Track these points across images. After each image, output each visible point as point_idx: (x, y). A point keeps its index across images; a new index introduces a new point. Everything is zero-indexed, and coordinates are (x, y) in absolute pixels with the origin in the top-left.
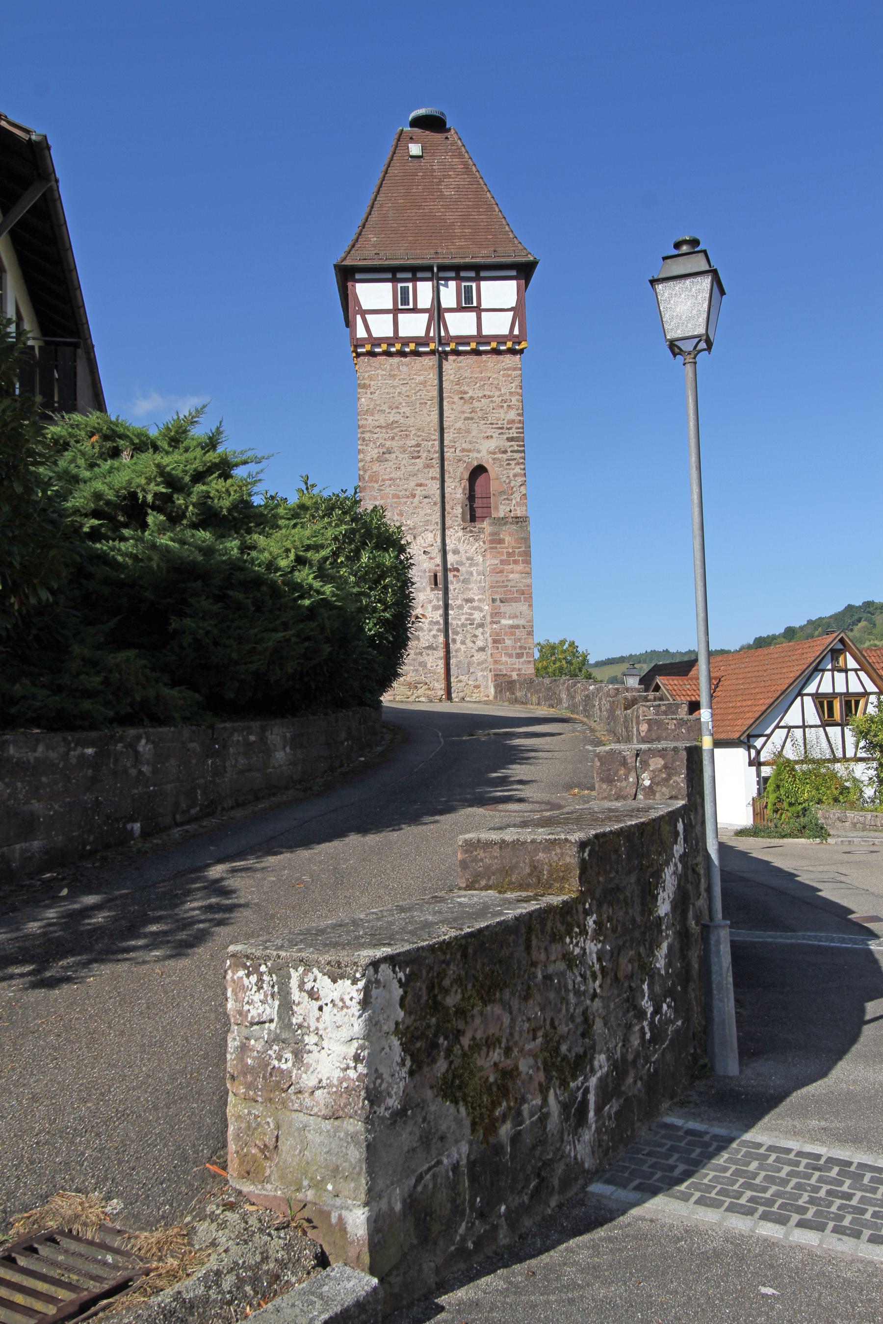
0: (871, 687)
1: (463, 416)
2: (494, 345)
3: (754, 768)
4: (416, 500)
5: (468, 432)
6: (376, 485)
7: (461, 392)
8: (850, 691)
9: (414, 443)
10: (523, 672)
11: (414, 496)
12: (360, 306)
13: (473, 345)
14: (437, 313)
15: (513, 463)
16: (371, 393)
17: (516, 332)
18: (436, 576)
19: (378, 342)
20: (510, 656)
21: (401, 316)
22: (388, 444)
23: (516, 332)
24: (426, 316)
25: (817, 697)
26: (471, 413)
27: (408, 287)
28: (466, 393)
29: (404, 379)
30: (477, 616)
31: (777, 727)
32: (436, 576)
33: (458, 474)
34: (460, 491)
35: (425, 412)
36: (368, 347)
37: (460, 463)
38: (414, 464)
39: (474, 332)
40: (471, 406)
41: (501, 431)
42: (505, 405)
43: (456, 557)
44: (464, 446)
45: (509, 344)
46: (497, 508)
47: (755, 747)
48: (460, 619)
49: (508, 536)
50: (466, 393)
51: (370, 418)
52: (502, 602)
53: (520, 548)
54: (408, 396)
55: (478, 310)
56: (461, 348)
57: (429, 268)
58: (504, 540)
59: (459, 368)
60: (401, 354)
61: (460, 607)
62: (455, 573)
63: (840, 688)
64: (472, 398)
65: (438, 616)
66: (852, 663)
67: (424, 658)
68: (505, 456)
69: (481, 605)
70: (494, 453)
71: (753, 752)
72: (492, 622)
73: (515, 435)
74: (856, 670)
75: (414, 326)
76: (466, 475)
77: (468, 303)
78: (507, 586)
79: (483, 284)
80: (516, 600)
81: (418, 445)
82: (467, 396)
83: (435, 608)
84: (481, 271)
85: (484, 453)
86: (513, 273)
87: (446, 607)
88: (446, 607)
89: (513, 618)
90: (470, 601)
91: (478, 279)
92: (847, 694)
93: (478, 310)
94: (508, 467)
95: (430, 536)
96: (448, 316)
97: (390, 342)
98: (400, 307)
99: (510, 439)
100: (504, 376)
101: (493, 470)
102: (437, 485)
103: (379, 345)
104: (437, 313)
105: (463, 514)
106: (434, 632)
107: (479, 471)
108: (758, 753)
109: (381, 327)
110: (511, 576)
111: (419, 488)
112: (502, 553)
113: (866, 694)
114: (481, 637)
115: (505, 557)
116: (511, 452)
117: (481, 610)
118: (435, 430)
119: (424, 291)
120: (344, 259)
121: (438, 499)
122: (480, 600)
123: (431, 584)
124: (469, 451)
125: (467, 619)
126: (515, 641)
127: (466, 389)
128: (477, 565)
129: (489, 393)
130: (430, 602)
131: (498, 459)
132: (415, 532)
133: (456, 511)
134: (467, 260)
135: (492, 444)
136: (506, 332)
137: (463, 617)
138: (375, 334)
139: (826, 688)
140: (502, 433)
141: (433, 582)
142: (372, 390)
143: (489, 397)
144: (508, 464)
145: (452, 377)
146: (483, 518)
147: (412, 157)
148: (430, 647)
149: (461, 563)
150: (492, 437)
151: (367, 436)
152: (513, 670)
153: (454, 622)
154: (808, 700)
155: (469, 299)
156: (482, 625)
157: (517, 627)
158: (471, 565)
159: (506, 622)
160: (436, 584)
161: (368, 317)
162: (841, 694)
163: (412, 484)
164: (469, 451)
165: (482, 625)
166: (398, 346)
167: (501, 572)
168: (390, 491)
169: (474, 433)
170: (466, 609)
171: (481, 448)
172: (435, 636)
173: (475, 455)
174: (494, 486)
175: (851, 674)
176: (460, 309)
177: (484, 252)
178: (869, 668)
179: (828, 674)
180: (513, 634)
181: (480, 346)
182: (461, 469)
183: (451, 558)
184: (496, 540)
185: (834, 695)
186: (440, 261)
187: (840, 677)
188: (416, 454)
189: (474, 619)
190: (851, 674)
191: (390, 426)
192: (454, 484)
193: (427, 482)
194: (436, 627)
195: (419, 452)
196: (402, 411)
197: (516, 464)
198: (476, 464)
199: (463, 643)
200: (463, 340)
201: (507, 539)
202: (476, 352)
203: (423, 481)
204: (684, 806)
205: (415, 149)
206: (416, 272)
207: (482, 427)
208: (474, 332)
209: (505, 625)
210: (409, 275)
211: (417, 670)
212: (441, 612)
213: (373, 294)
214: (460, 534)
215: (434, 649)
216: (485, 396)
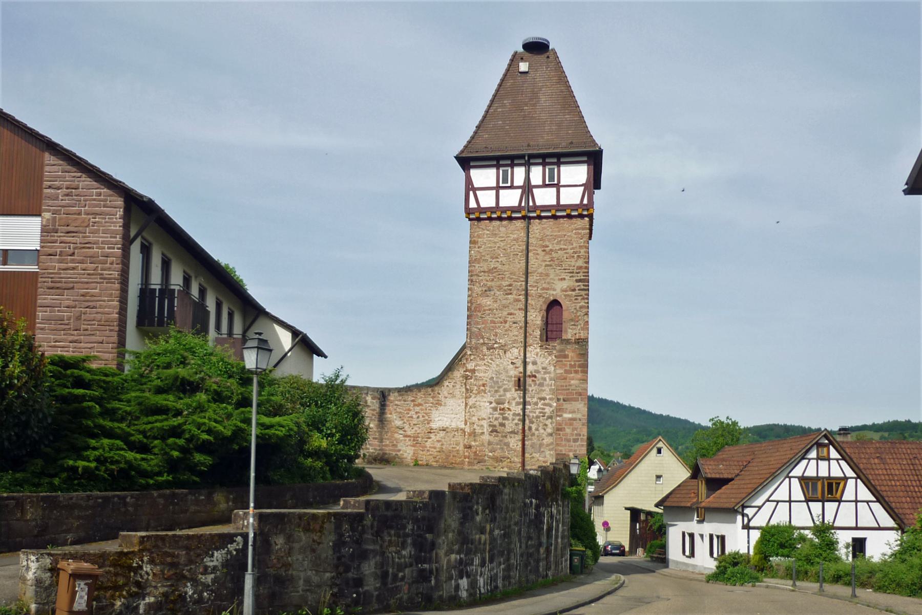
0: (850, 473)
1: (544, 264)
2: (568, 211)
3: (746, 531)
4: (507, 325)
5: (547, 275)
6: (479, 314)
7: (544, 246)
8: (832, 475)
9: (507, 283)
11: (506, 322)
12: (473, 185)
13: (553, 212)
14: (527, 189)
15: (580, 298)
17: (585, 202)
18: (519, 380)
19: (484, 210)
21: (501, 192)
22: (489, 284)
23: (585, 202)
24: (520, 191)
25: (803, 480)
30: (548, 410)
31: (768, 500)
32: (519, 380)
33: (538, 307)
34: (540, 318)
35: (517, 261)
36: (477, 215)
37: (541, 299)
38: (507, 299)
39: (554, 203)
43: (535, 367)
44: (544, 285)
46: (566, 332)
47: (747, 516)
49: (571, 353)
51: (477, 265)
52: (564, 400)
55: (558, 186)
56: (543, 214)
57: (522, 157)
59: (544, 228)
60: (500, 219)
61: (536, 404)
63: (823, 473)
64: (551, 250)
65: (519, 409)
66: (834, 454)
67: (508, 440)
68: (574, 293)
70: (566, 291)
71: (746, 519)
72: (557, 416)
74: (837, 460)
75: (510, 198)
76: (545, 307)
80: (576, 400)
81: (510, 285)
82: (547, 249)
83: (518, 404)
85: (558, 290)
86: (585, 159)
87: (525, 403)
88: (525, 403)
90: (544, 399)
91: (559, 164)
92: (829, 478)
93: (558, 186)
95: (515, 351)
96: (535, 190)
97: (491, 210)
98: (501, 185)
99: (577, 281)
100: (575, 234)
101: (565, 303)
102: (522, 314)
103: (505, 212)
104: (527, 189)
105: (541, 335)
106: (516, 421)
107: (554, 305)
108: (749, 520)
109: (487, 200)
110: (572, 382)
112: (565, 365)
113: (846, 479)
114: (550, 426)
115: (568, 368)
117: (551, 406)
119: (519, 174)
120: (462, 152)
121: (522, 324)
122: (550, 399)
124: (548, 289)
126: (574, 429)
127: (547, 243)
128: (549, 373)
129: (562, 247)
130: (514, 399)
131: (568, 295)
133: (536, 333)
135: (565, 285)
136: (578, 202)
137: (537, 411)
138: (482, 205)
139: (811, 472)
145: (537, 235)
146: (554, 339)
147: (521, 73)
148: (513, 432)
149: (538, 372)
150: (564, 279)
152: (570, 451)
153: (531, 415)
154: (795, 483)
155: (552, 178)
156: (550, 417)
157: (574, 419)
158: (545, 373)
159: (567, 416)
160: (519, 386)
161: (478, 192)
162: (823, 478)
163: (505, 313)
164: (548, 289)
165: (550, 417)
166: (499, 214)
167: (565, 379)
168: (489, 318)
170: (540, 405)
171: (556, 287)
172: (516, 424)
173: (552, 292)
174: (566, 315)
175: (833, 463)
176: (545, 185)
178: (847, 458)
179: (813, 462)
180: (571, 424)
182: (541, 303)
183: (530, 368)
184: (562, 356)
185: (818, 478)
187: (823, 465)
190: (833, 463)
191: (490, 271)
198: (552, 298)
199: (537, 429)
202: (555, 217)
203: (512, 311)
204: (123, 531)
205: (523, 67)
206: (513, 160)
207: (558, 272)
208: (554, 203)
210: (509, 162)
211: (502, 449)
212: (521, 407)
213: (484, 177)
214: (538, 350)
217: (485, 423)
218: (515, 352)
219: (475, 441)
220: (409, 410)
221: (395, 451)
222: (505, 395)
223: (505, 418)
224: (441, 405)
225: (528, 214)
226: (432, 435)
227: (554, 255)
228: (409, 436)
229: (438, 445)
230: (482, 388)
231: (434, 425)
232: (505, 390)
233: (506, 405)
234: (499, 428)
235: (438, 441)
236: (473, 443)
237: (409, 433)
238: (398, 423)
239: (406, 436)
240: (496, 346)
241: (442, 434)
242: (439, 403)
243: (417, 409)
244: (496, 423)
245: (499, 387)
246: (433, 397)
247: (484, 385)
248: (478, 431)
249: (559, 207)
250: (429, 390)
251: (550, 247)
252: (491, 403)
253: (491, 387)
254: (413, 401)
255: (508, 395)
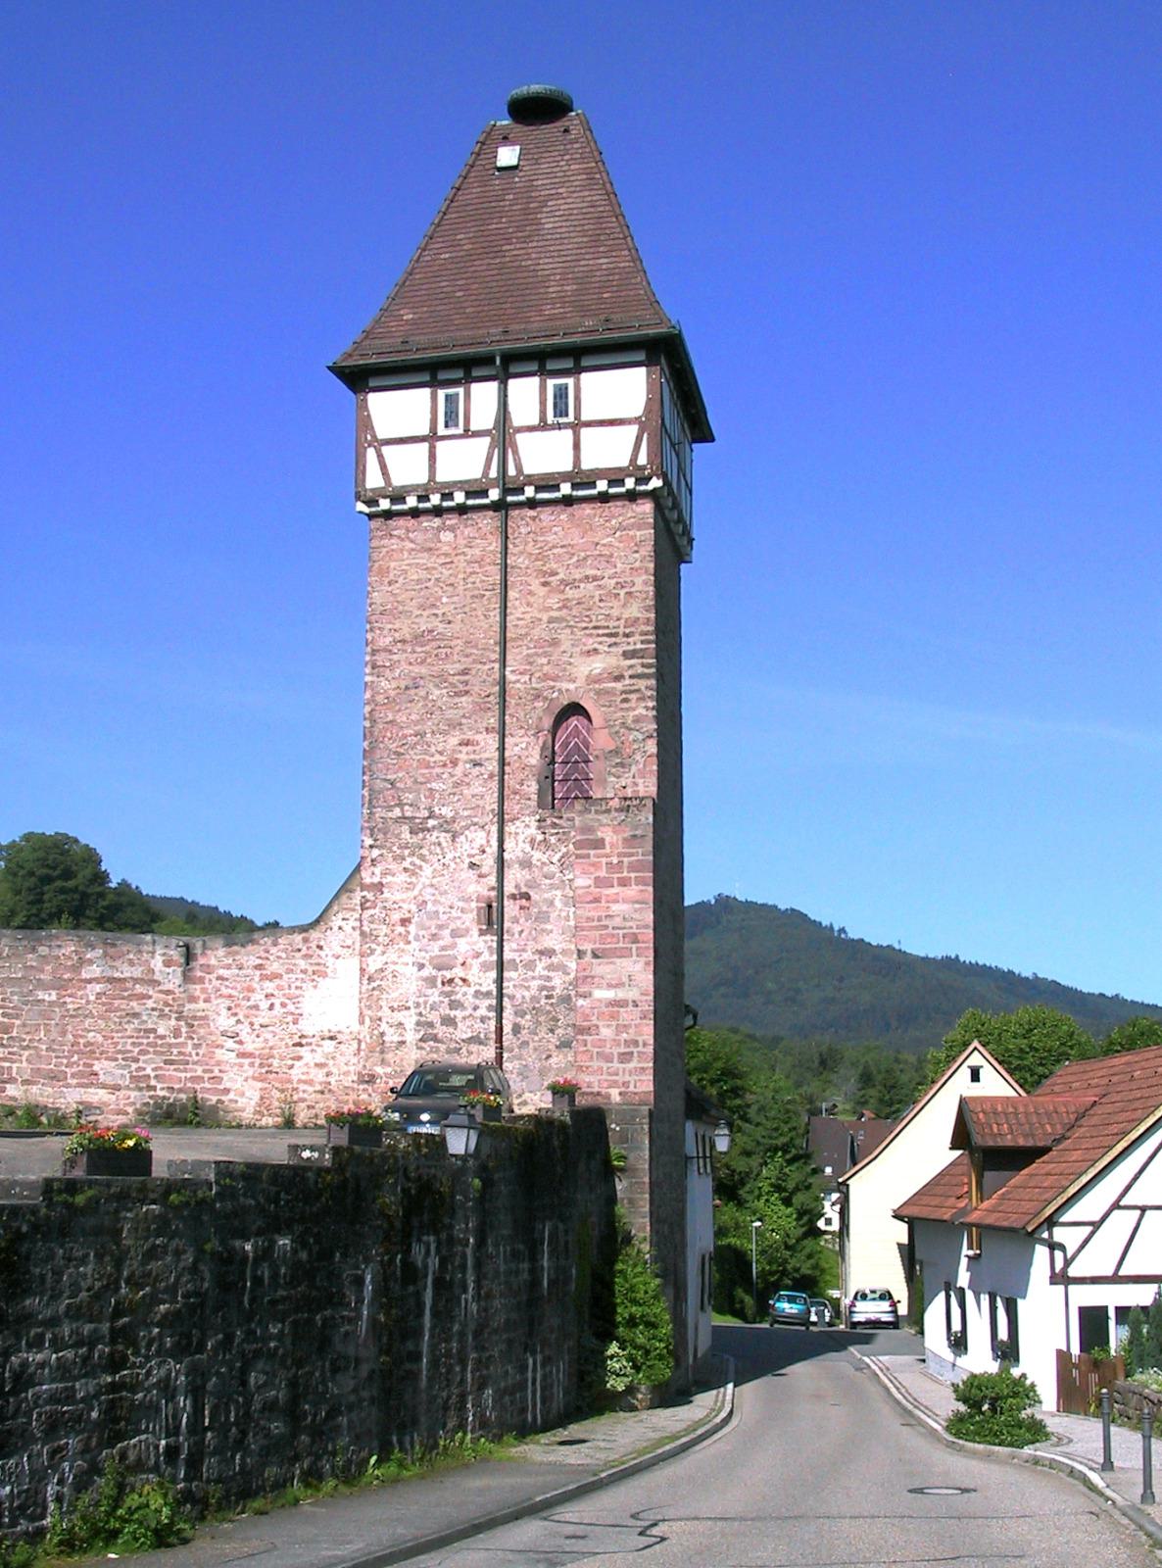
4: (459, 771)
5: (555, 643)
9: (459, 667)
10: (631, 1088)
11: (455, 763)
12: (374, 436)
14: (503, 434)
15: (633, 697)
16: (390, 583)
18: (490, 907)
20: (609, 1059)
23: (642, 460)
24: (487, 440)
26: (560, 609)
27: (566, 385)
28: (554, 574)
29: (446, 555)
32: (490, 907)
40: (562, 597)
41: (613, 640)
42: (622, 593)
45: (630, 483)
48: (528, 988)
50: (554, 574)
52: (595, 956)
53: (632, 855)
54: (452, 585)
57: (486, 360)
58: (602, 840)
62: (524, 902)
64: (564, 583)
68: (619, 686)
69: (564, 960)
73: (639, 646)
75: (464, 461)
77: (562, 414)
78: (606, 927)
79: (585, 377)
80: (625, 954)
81: (465, 672)
84: (580, 356)
86: (641, 356)
87: (500, 966)
88: (500, 966)
89: (616, 986)
91: (577, 371)
94: (625, 705)
95: (479, 837)
96: (520, 438)
99: (626, 655)
102: (492, 741)
104: (503, 434)
105: (540, 793)
106: (482, 1012)
109: (407, 468)
110: (615, 908)
111: (464, 749)
115: (603, 873)
116: (631, 677)
118: (496, 643)
119: (483, 397)
122: (564, 952)
123: (479, 922)
125: (542, 988)
130: (478, 955)
132: (456, 827)
134: (556, 341)
135: (598, 665)
136: (624, 462)
140: (615, 644)
141: (484, 919)
142: (391, 576)
143: (595, 579)
144: (625, 700)
151: (380, 659)
152: (613, 1084)
159: (602, 994)
160: (490, 923)
161: (385, 450)
163: (453, 741)
167: (597, 900)
169: (566, 645)
172: (483, 1020)
176: (543, 426)
177: (589, 323)
180: (613, 1016)
181: (580, 490)
186: (507, 346)
188: (461, 687)
189: (553, 988)
191: (418, 638)
192: (526, 739)
193: (479, 737)
194: (487, 1002)
195: (466, 683)
196: (440, 612)
197: (638, 699)
200: (547, 483)
201: (608, 840)
203: (469, 735)
205: (507, 156)
206: (467, 367)
209: (600, 1000)
212: (493, 974)
213: (397, 410)
215: (481, 1043)
216: (587, 577)
217: (410, 1019)
218: (479, 839)
219: (383, 1062)
220: (251, 990)
221: (216, 1091)
222: (453, 946)
223: (455, 1005)
224: (324, 975)
225: (507, 498)
226: (302, 1051)
227: (570, 593)
228: (250, 1055)
229: (319, 1076)
230: (401, 929)
231: (307, 1026)
232: (455, 934)
233: (458, 972)
234: (441, 1030)
235: (319, 1065)
236: (379, 1070)
237: (249, 1047)
238: (224, 1022)
239: (242, 1055)
240: (431, 823)
241: (329, 1045)
242: (320, 972)
243: (269, 986)
244: (434, 1017)
245: (440, 927)
246: (307, 956)
247: (405, 922)
248: (392, 1037)
249: (582, 479)
250: (298, 938)
251: (561, 576)
252: (421, 967)
253: (421, 926)
254: (259, 967)
255: (463, 946)
